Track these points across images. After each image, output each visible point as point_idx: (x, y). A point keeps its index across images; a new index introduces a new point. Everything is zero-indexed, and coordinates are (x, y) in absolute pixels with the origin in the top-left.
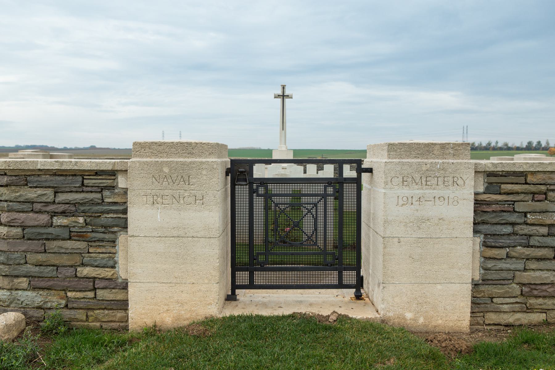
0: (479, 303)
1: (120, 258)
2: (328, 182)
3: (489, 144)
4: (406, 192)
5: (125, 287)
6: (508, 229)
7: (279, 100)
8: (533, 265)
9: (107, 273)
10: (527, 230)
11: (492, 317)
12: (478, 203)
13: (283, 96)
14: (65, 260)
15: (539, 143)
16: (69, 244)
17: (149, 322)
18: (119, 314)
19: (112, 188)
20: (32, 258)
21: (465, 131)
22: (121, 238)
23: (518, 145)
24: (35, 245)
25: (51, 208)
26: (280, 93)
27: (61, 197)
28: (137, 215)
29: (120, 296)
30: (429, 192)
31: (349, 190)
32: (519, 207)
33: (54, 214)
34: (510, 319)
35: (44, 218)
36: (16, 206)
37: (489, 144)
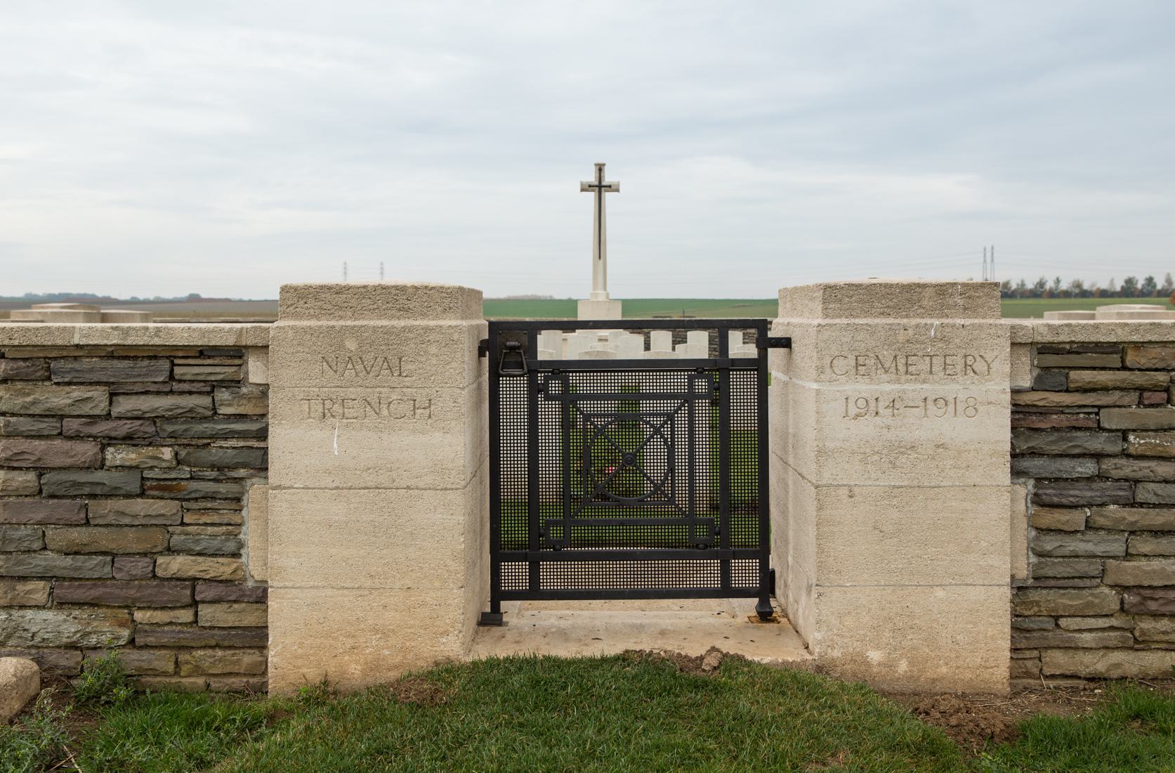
0: (1029, 628)
1: (250, 534)
2: (696, 368)
4: (863, 388)
5: (261, 597)
6: (1088, 468)
9: (220, 568)
10: (1129, 468)
11: (1059, 661)
13: (600, 187)
14: (130, 540)
15: (1150, 280)
16: (140, 506)
17: (313, 674)
18: (248, 658)
19: (234, 383)
21: (989, 255)
22: (254, 491)
23: (1104, 285)
24: (67, 508)
25: (102, 428)
26: (592, 178)
27: (125, 405)
28: (289, 441)
29: (250, 619)
30: (913, 389)
32: (1111, 420)
33: (108, 441)
34: (1099, 663)
35: (86, 450)
36: (25, 425)
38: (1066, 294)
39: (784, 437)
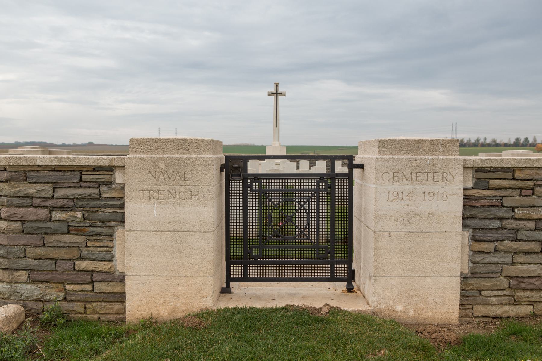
1: (117, 252)
2: (320, 177)
3: (478, 140)
4: (397, 187)
5: (122, 280)
6: (496, 224)
7: (273, 98)
8: (520, 259)
9: (104, 266)
10: (514, 224)
11: (480, 310)
12: (466, 198)
13: (277, 94)
14: (63, 254)
16: (68, 238)
17: (146, 314)
18: (117, 307)
19: (109, 183)
20: (32, 252)
21: (455, 127)
22: (119, 232)
23: (506, 141)
24: (35, 239)
25: (50, 203)
26: (273, 90)
27: (60, 193)
28: (134, 209)
29: (117, 289)
30: (419, 188)
31: (341, 186)
32: (507, 202)
33: (53, 209)
34: (498, 311)
35: (43, 213)
37: (478, 140)
38: (489, 145)
39: (360, 210)
